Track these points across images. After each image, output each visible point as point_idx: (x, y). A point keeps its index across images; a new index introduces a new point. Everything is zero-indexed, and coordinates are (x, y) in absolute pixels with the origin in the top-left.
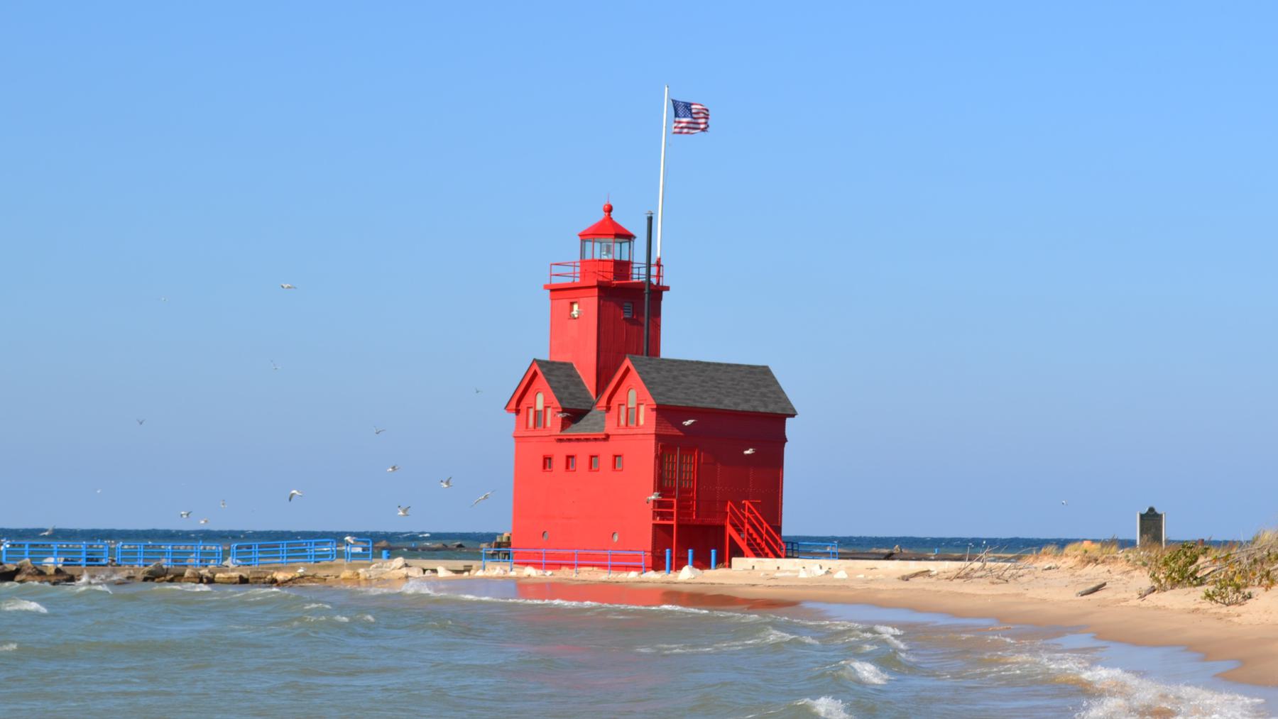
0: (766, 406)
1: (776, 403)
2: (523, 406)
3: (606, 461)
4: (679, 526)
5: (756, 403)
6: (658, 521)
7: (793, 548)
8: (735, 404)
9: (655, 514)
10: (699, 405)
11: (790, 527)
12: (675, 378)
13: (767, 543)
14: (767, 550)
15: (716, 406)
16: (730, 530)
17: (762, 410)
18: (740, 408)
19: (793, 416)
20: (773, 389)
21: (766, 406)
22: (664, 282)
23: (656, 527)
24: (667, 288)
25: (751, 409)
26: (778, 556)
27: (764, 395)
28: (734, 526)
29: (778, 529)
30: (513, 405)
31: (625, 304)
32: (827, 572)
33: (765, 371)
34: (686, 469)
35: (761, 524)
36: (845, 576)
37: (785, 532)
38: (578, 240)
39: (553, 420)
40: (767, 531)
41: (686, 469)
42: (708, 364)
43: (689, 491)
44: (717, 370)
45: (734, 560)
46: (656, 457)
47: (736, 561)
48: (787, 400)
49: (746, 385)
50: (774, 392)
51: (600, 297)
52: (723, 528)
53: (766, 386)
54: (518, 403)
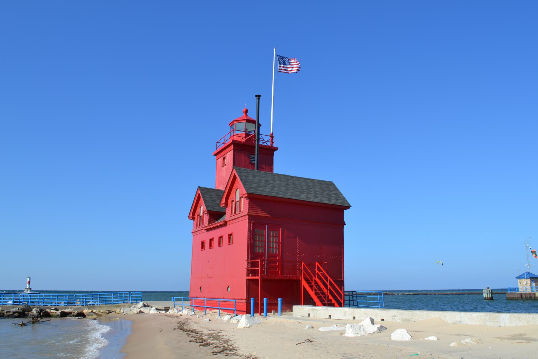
0: (330, 201)
1: (337, 200)
2: (196, 216)
3: (225, 239)
4: (263, 280)
5: (322, 199)
6: (251, 277)
7: (354, 300)
8: (308, 197)
9: (249, 272)
10: (280, 196)
11: (352, 281)
12: (266, 181)
13: (331, 293)
14: (333, 301)
15: (294, 198)
16: (304, 283)
17: (327, 202)
18: (311, 200)
19: (348, 207)
20: (335, 192)
21: (330, 201)
22: (275, 145)
23: (249, 281)
24: (276, 149)
25: (319, 201)
26: (340, 305)
27: (329, 195)
28: (306, 280)
29: (341, 283)
30: (191, 215)
31: (252, 152)
32: (381, 328)
33: (331, 184)
34: (272, 241)
35: (327, 279)
36: (407, 337)
37: (347, 288)
38: (229, 126)
39: (206, 218)
40: (331, 284)
41: (272, 241)
42: (292, 177)
43: (276, 256)
44: (298, 180)
45: (294, 307)
46: (249, 231)
47: (300, 310)
48: (344, 199)
49: (317, 189)
50: (336, 194)
51: (234, 150)
52: (299, 282)
53: (331, 191)
54: (193, 215)
